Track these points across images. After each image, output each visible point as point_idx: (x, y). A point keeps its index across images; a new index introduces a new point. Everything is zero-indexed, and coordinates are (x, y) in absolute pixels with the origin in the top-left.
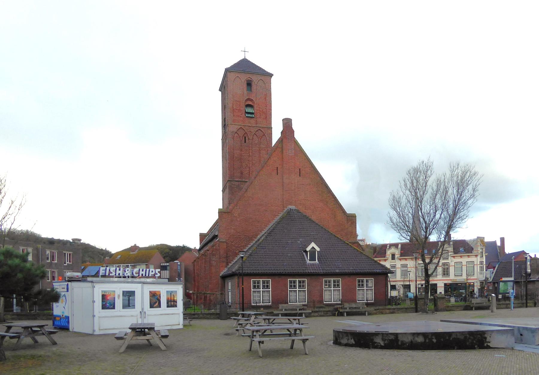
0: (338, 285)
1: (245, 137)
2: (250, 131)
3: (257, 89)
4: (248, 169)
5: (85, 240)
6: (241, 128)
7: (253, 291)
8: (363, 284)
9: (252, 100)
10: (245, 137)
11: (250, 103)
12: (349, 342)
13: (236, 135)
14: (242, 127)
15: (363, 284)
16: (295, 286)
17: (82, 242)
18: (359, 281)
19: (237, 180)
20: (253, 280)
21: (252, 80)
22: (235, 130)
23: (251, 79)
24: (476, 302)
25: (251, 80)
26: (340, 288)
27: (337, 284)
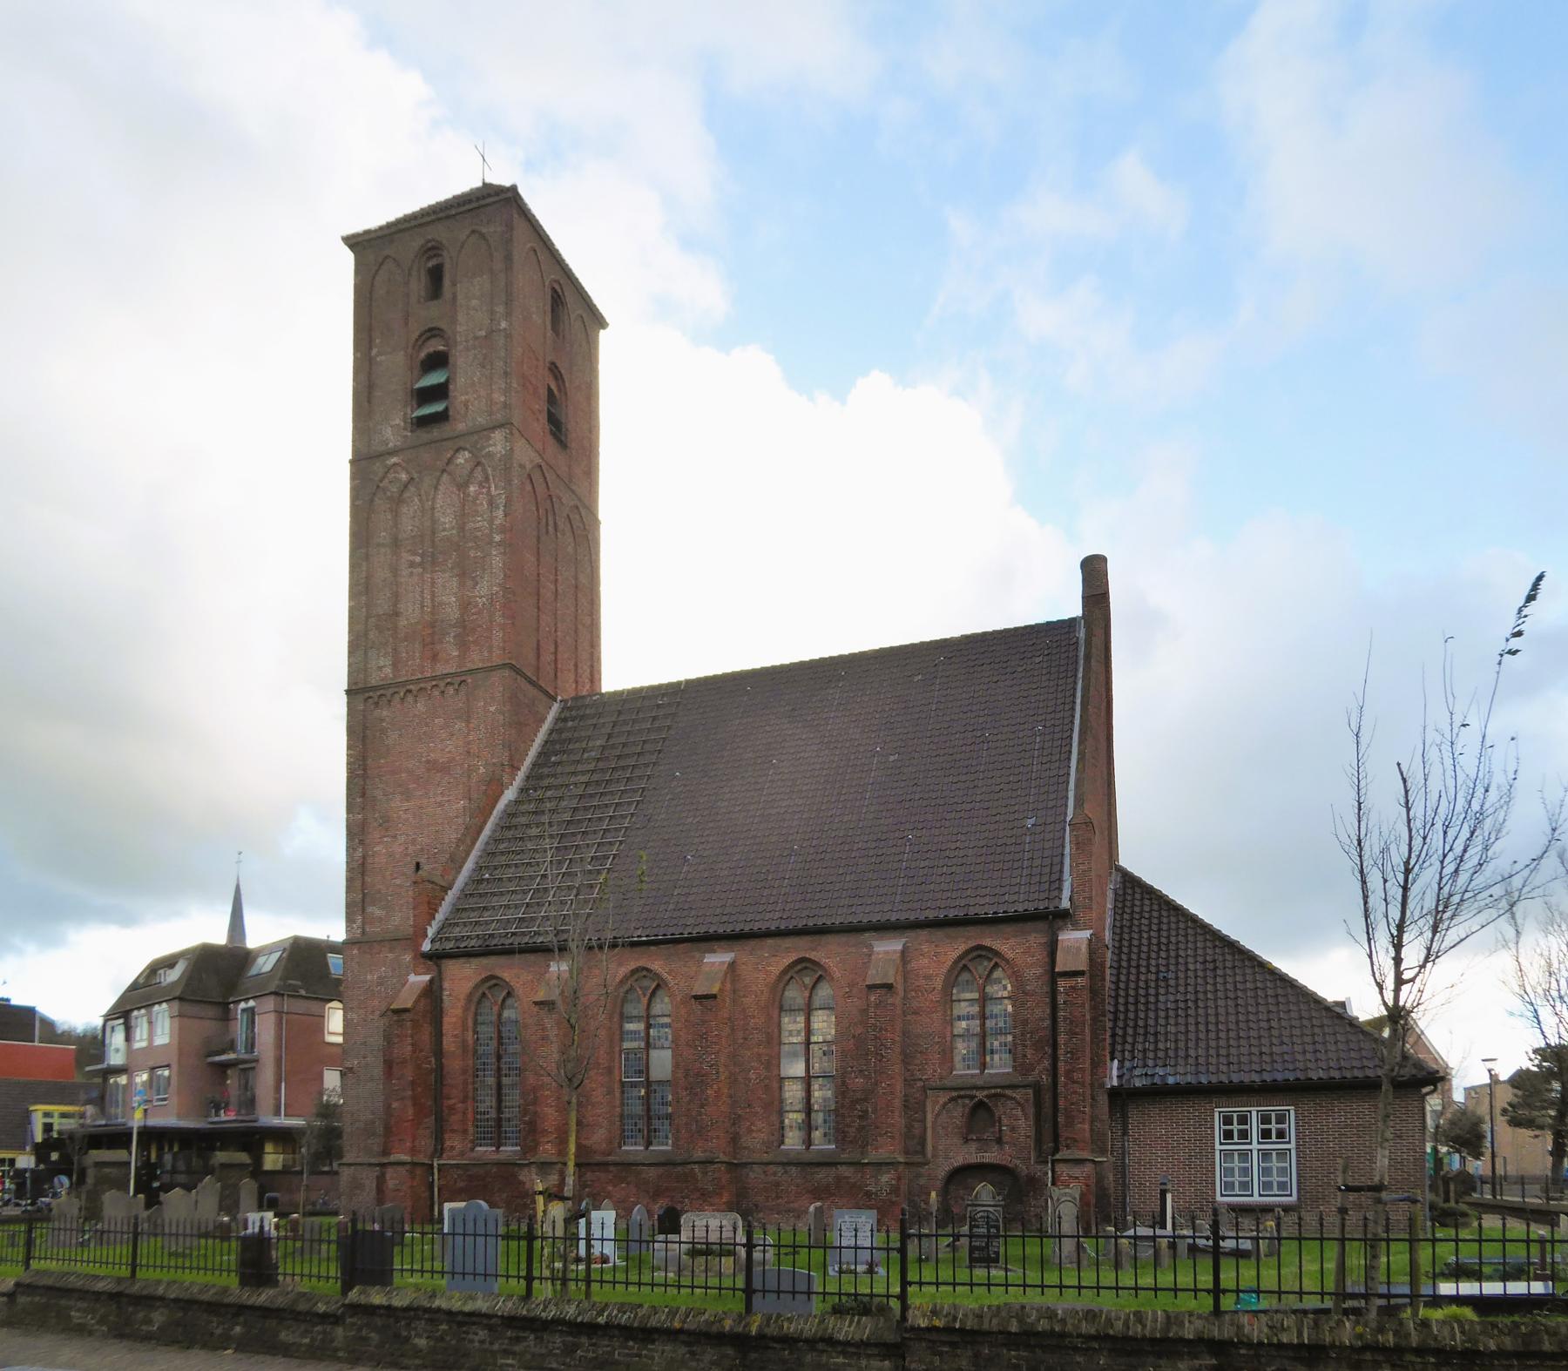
2: (560, 499)
4: (552, 649)
7: (1221, 1151)
16: (1244, 1135)
18: (1227, 1120)
23: (562, 289)
25: (559, 296)
27: (1277, 1129)
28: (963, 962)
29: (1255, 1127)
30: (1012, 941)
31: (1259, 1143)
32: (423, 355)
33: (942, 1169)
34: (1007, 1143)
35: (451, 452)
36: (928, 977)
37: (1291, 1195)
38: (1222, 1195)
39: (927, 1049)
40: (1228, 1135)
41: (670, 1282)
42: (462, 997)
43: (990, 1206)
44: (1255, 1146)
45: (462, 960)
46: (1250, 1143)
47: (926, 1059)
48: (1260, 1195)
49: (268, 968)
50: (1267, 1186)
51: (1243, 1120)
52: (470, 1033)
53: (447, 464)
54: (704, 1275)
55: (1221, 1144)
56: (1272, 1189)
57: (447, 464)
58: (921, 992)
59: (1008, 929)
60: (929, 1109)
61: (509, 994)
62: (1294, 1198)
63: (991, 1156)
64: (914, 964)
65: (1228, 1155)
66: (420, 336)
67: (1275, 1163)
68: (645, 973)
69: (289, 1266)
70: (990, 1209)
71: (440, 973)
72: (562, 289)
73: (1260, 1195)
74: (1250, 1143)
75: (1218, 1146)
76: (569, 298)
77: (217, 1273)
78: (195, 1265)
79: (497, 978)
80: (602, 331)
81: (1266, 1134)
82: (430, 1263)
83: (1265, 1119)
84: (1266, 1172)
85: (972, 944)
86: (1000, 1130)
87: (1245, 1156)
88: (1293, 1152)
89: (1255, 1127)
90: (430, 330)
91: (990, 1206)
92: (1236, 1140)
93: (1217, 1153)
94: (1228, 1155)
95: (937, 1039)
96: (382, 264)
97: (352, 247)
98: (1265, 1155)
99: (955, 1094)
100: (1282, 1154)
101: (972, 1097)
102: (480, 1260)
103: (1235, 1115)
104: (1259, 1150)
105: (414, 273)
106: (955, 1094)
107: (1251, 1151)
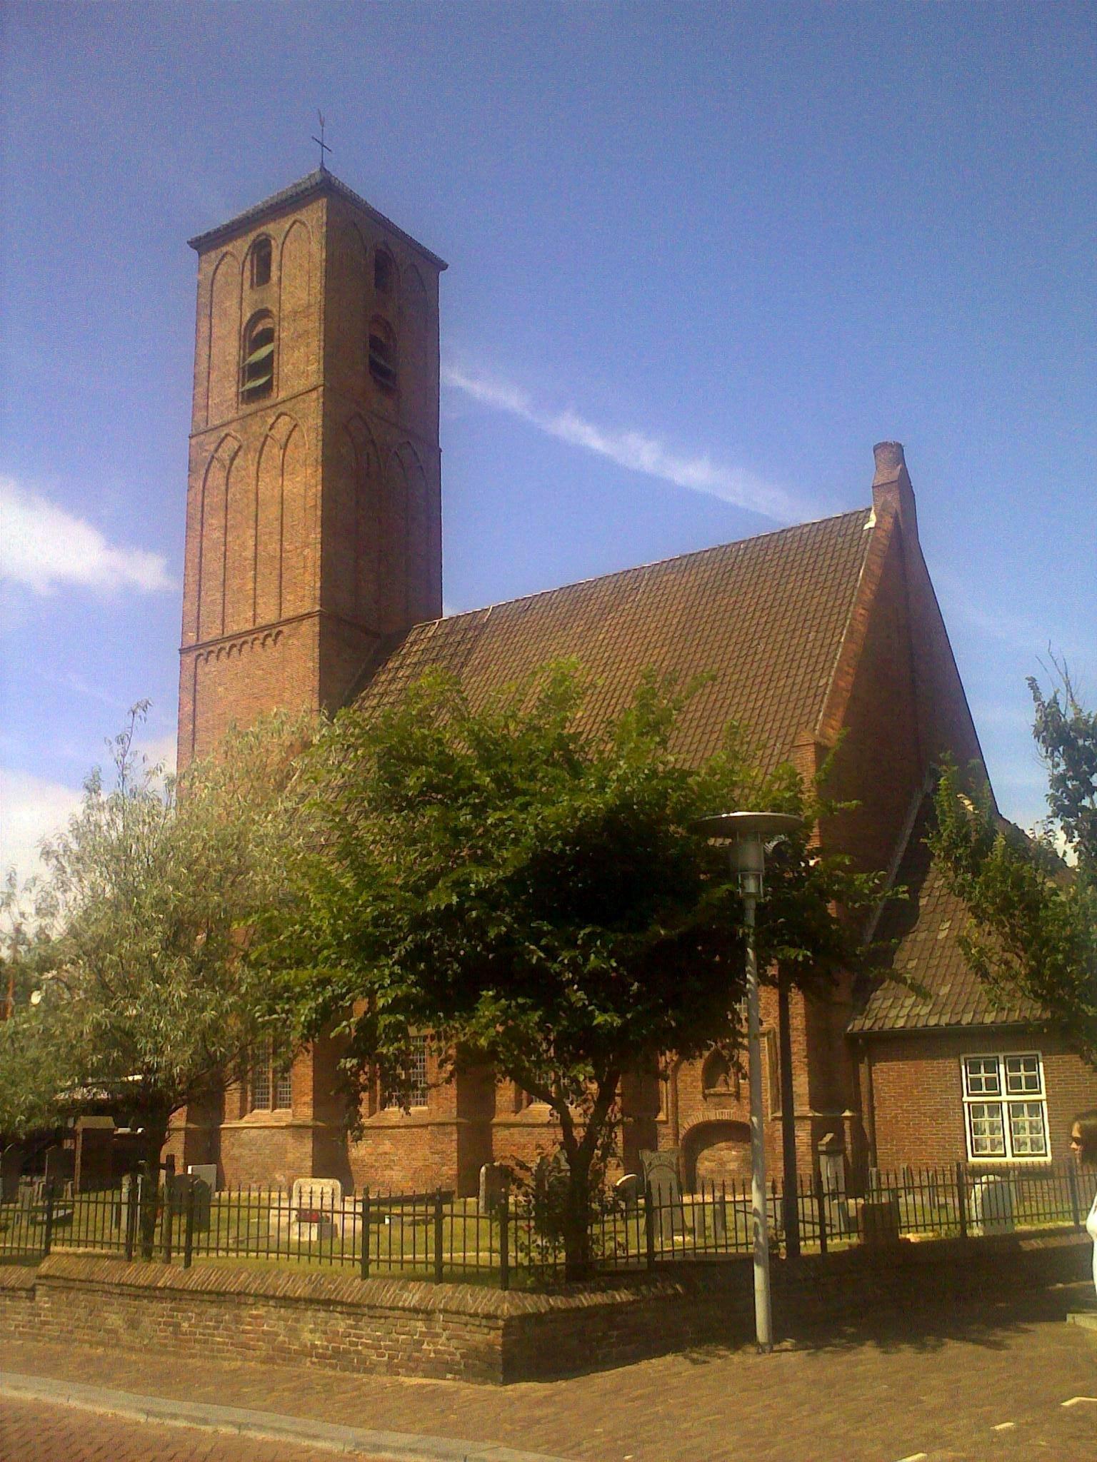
23: (246, 258)
26: (1040, 1093)
31: (1008, 1093)
33: (688, 1122)
35: (274, 418)
41: (231, 1246)
44: (1004, 1097)
48: (1014, 1156)
49: (829, 905)
53: (270, 429)
57: (270, 429)
62: (1049, 1159)
63: (728, 1113)
65: (977, 1110)
69: (284, 1220)
72: (246, 258)
73: (1014, 1156)
74: (1040, 1093)
77: (1002, 1221)
78: (234, 1212)
88: (1044, 1103)
93: (966, 1105)
96: (222, 259)
98: (1016, 1109)
100: (1035, 1108)
102: (994, 1210)
104: (1009, 1102)
107: (1001, 1102)
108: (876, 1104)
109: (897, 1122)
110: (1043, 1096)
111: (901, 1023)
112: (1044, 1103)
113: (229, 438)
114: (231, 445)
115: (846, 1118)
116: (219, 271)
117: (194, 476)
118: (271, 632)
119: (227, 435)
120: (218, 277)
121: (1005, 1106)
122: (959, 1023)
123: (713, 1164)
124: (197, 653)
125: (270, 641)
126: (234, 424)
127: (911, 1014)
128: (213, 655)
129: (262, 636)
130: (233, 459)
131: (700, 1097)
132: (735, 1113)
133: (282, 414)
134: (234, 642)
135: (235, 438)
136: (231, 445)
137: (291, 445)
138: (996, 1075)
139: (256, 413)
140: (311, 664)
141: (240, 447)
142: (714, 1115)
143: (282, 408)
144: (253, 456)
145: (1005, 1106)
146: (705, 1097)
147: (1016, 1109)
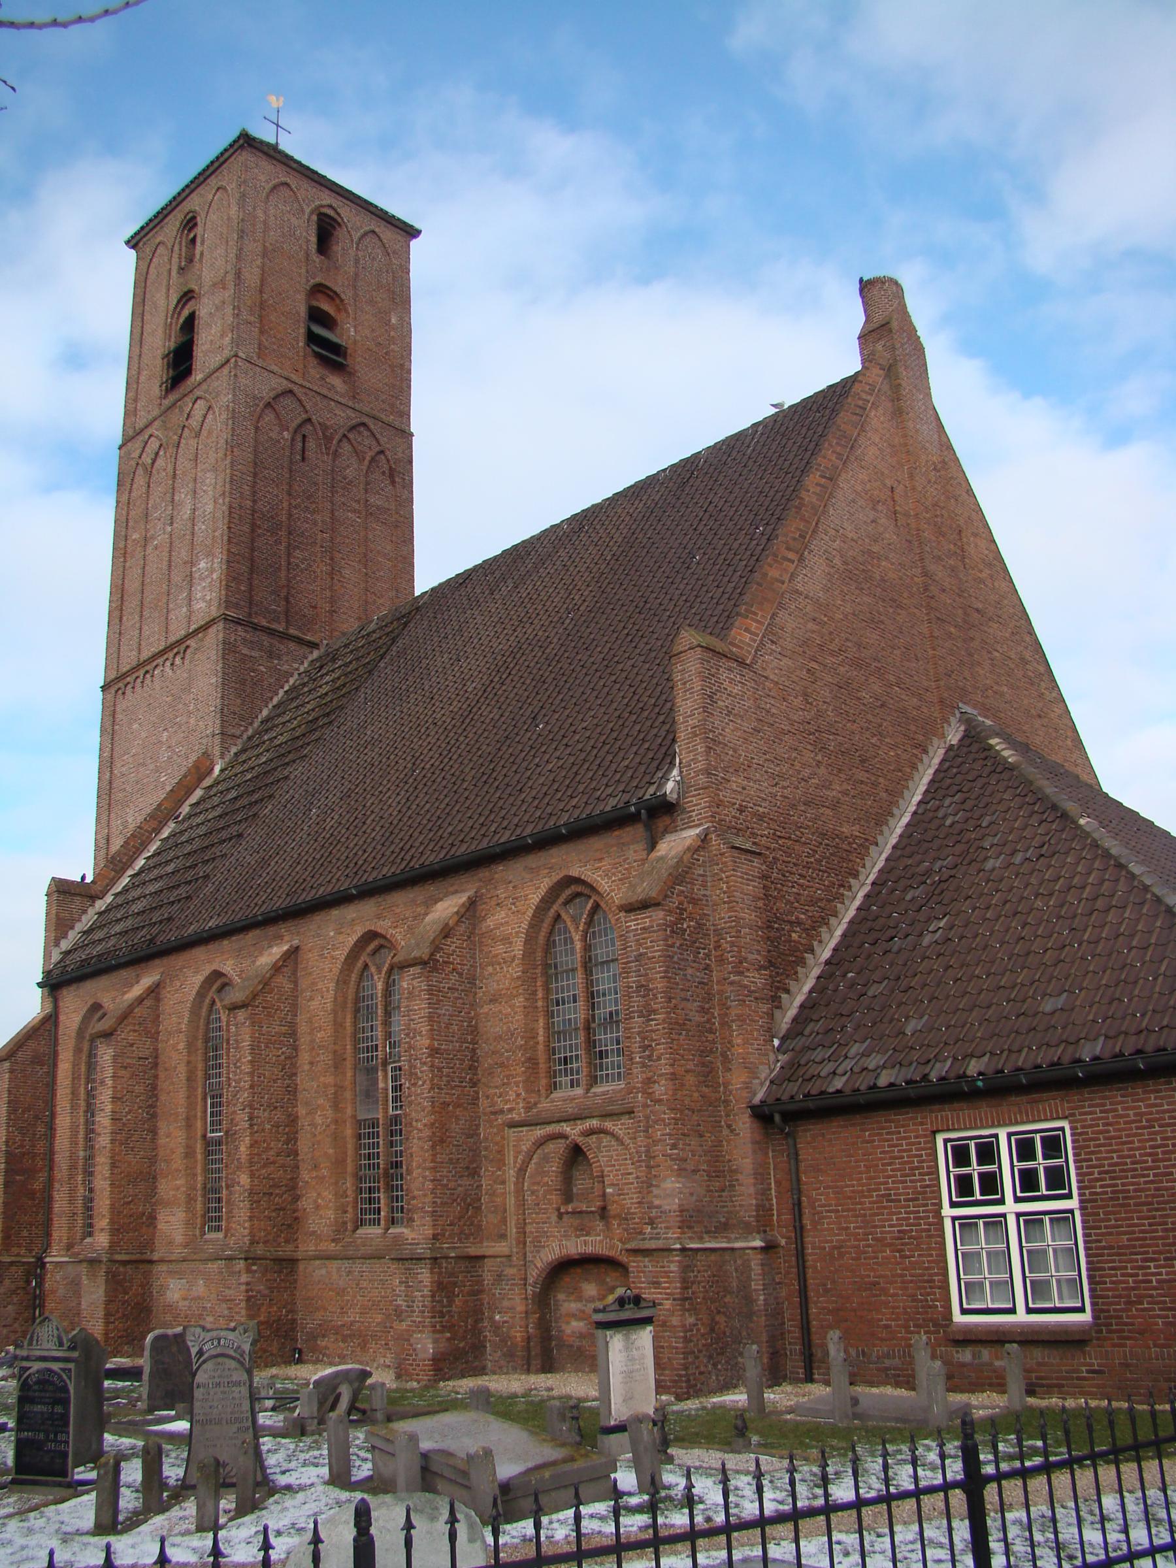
0: (1057, 1178)
1: (304, 436)
3: (357, 261)
5: (792, 398)
6: (291, 391)
7: (954, 1219)
8: (957, 1164)
9: (335, 293)
10: (304, 436)
11: (326, 306)
12: (719, 1455)
13: (269, 417)
14: (295, 389)
15: (957, 1164)
16: (991, 1184)
17: (786, 407)
18: (960, 1156)
19: (264, 623)
20: (946, 1141)
21: (339, 220)
22: (266, 394)
23: (338, 214)
24: (555, 1198)
26: (1069, 1196)
27: (1047, 1170)
28: (555, 907)
29: (1007, 1166)
30: (606, 864)
31: (1017, 1200)
32: (181, 320)
34: (614, 1217)
36: (506, 940)
37: (1081, 1310)
38: (964, 1312)
39: (508, 1058)
40: (964, 1186)
42: (74, 1034)
43: (56, 1359)
44: (1010, 1207)
45: (74, 986)
46: (1001, 1202)
47: (508, 1077)
48: (1029, 1311)
50: (1038, 1289)
51: (988, 1153)
52: (83, 1082)
54: (1143, 1524)
55: (953, 1205)
56: (983, 1298)
58: (499, 964)
59: (596, 843)
60: (510, 1158)
61: (596, 907)
62: (1086, 1317)
64: (490, 922)
65: (966, 1225)
66: (179, 302)
67: (982, 1242)
68: (579, 889)
70: (55, 1366)
71: (56, 1007)
73: (1029, 1311)
74: (1001, 1202)
75: (947, 1211)
76: (346, 213)
79: (578, 881)
80: (414, 244)
81: (1028, 1180)
82: (849, 1481)
83: (1025, 1149)
84: (1034, 1259)
85: (556, 877)
86: (604, 1194)
87: (996, 1223)
88: (1077, 1214)
89: (1007, 1166)
90: (186, 294)
91: (56, 1359)
92: (978, 1196)
93: (948, 1224)
94: (966, 1225)
95: (520, 1042)
97: (133, 247)
98: (1031, 1222)
99: (540, 1132)
100: (1062, 1219)
101: (563, 1136)
103: (1038, 1137)
104: (1018, 1215)
105: (176, 248)
106: (540, 1132)
107: (1004, 1215)
108: (807, 1222)
109: (841, 1255)
110: (1073, 1203)
111: (838, 1083)
112: (1077, 1214)
113: (152, 439)
114: (153, 445)
115: (172, 1437)
116: (153, 265)
117: (122, 488)
118: (177, 648)
119: (151, 436)
120: (152, 270)
121: (1011, 1221)
122: (925, 1077)
123: (581, 1324)
124: (117, 687)
125: (178, 661)
126: (156, 423)
127: (856, 1069)
128: (130, 686)
129: (171, 655)
130: (154, 461)
131: (554, 1218)
132: (601, 1242)
133: (198, 398)
134: (147, 668)
135: (157, 437)
136: (153, 445)
137: (204, 433)
138: (1038, 1137)
139: (174, 404)
140: (214, 680)
141: (161, 445)
142: (575, 1247)
143: (198, 393)
144: (172, 450)
145: (1011, 1221)
146: (560, 1216)
147: (1031, 1222)
